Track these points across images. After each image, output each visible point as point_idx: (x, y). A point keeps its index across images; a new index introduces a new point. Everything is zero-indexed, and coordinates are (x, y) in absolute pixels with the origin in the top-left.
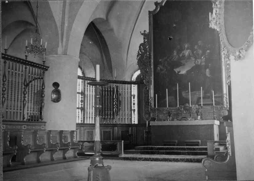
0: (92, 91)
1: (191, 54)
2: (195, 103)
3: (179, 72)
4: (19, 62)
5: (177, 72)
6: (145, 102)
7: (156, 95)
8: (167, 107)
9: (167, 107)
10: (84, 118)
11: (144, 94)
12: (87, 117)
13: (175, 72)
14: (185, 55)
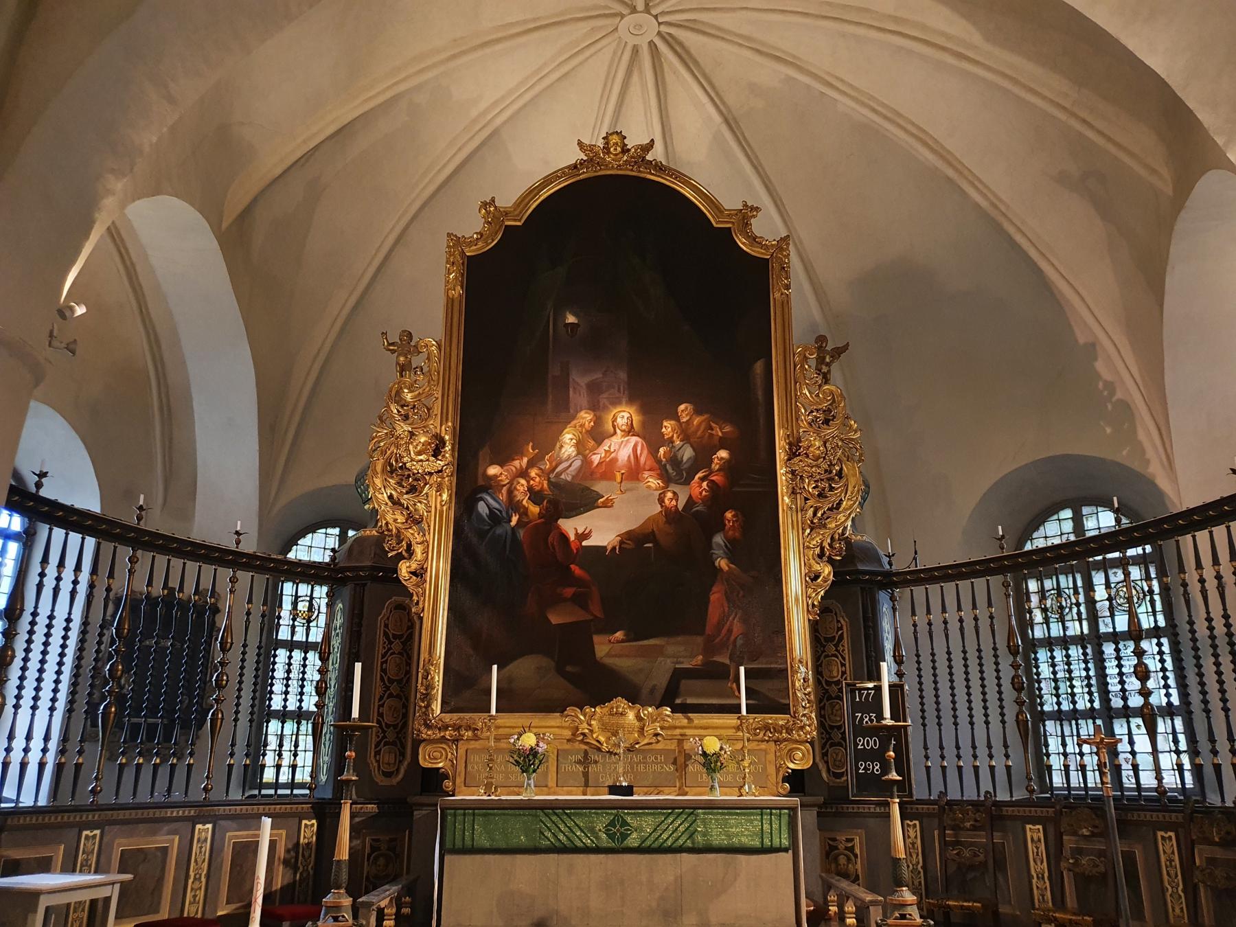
0: (29, 737)
1: (642, 460)
2: (658, 695)
3: (585, 536)
4: (81, 811)
5: (572, 538)
6: (382, 679)
7: (358, 666)
8: (493, 711)
9: (493, 711)
10: (791, 63)
11: (381, 639)
12: (1216, 561)
13: (564, 537)
14: (615, 460)
